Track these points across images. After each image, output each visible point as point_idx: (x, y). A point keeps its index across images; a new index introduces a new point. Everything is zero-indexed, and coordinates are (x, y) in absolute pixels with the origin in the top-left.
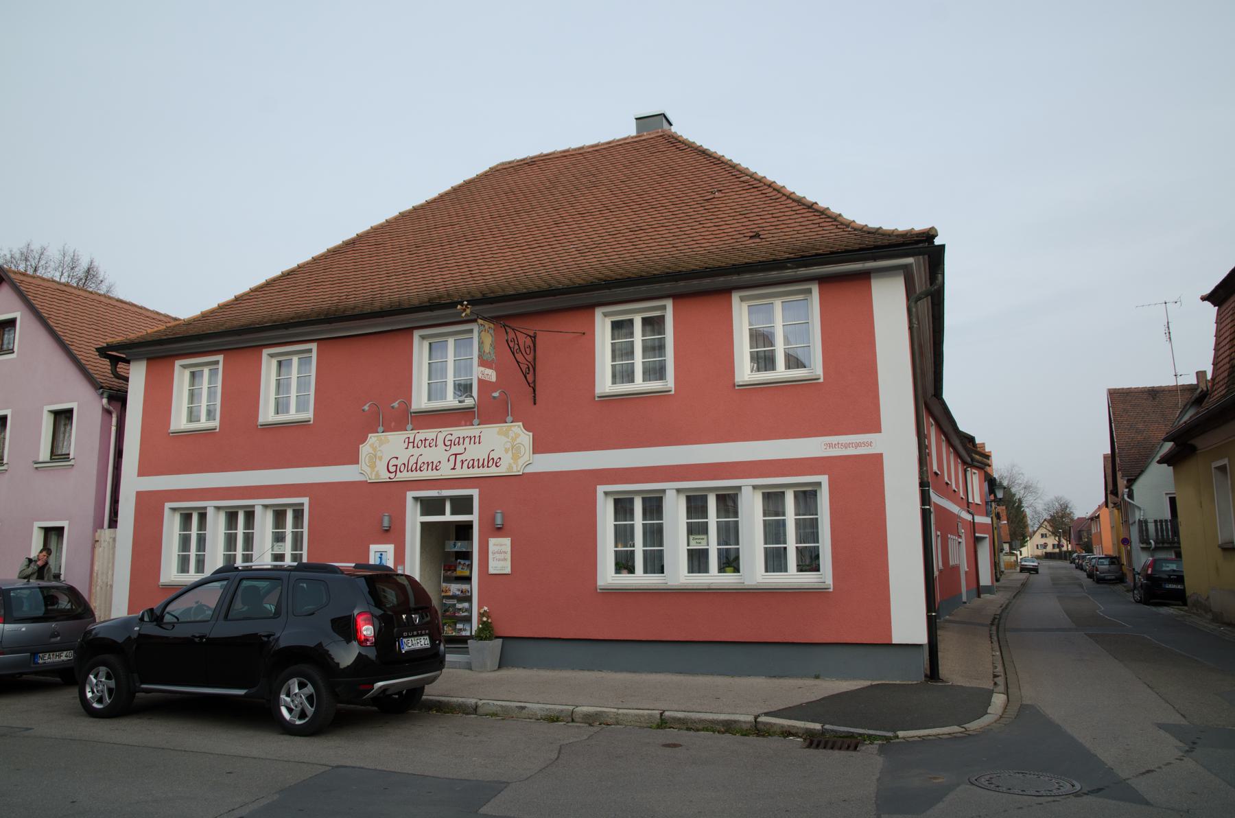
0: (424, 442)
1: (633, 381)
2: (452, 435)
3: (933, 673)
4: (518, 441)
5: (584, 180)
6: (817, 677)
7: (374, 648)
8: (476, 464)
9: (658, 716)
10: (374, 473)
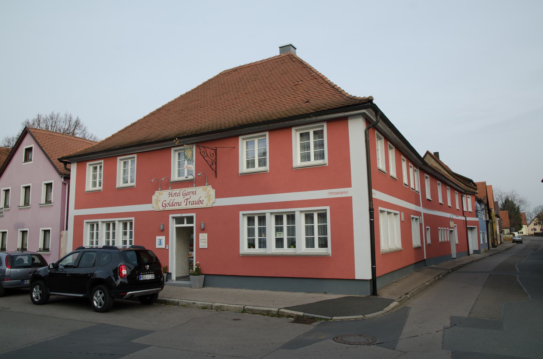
1: (254, 167)
3: (374, 292)
5: (253, 77)
6: (325, 293)
7: (127, 279)
9: (243, 308)
10: (157, 207)
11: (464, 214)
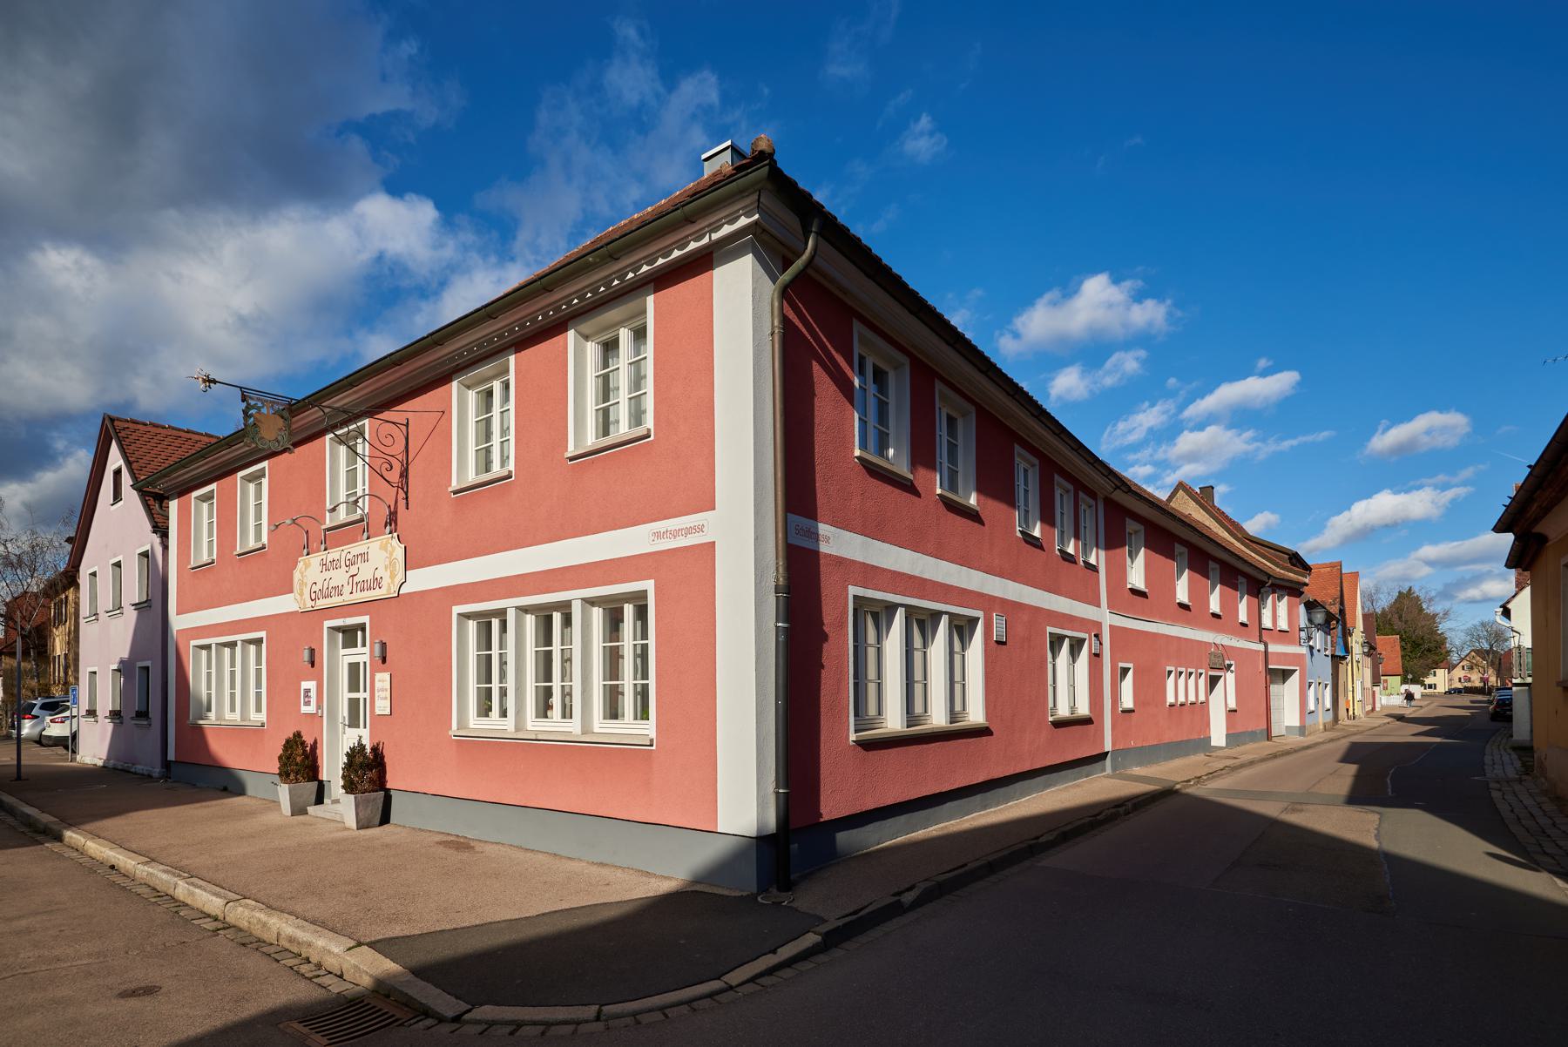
11: (1262, 634)
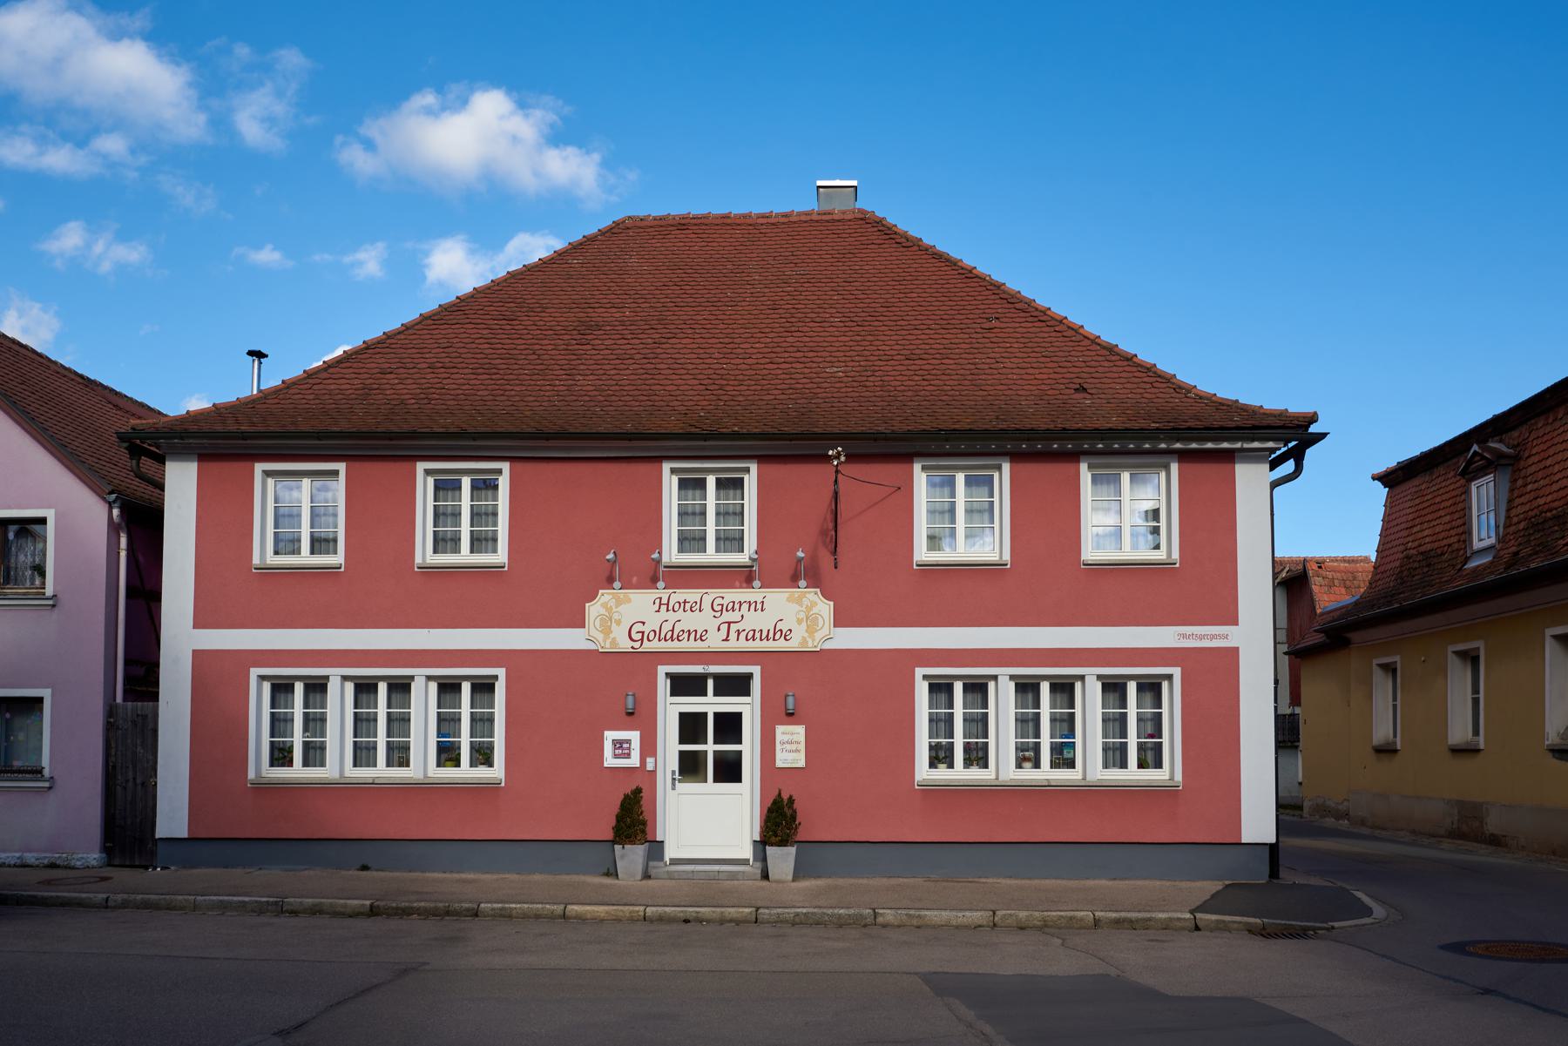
0: (682, 605)
2: (723, 598)
4: (815, 610)
8: (758, 635)
